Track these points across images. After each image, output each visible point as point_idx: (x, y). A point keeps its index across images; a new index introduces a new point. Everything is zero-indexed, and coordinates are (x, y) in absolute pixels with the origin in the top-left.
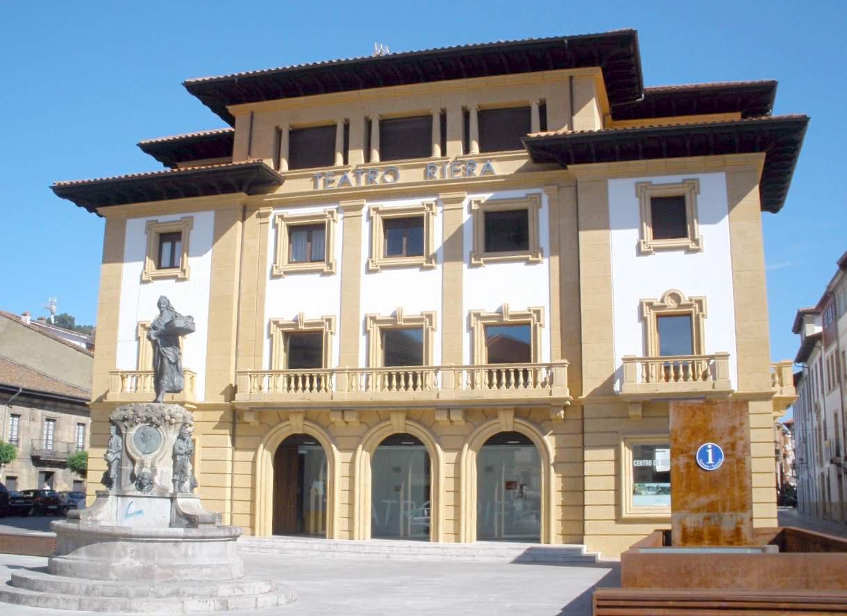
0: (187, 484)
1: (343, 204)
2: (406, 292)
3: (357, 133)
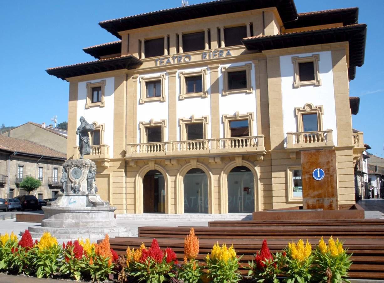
0: (93, 190)
1: (168, 71)
2: (196, 108)
3: (173, 40)
